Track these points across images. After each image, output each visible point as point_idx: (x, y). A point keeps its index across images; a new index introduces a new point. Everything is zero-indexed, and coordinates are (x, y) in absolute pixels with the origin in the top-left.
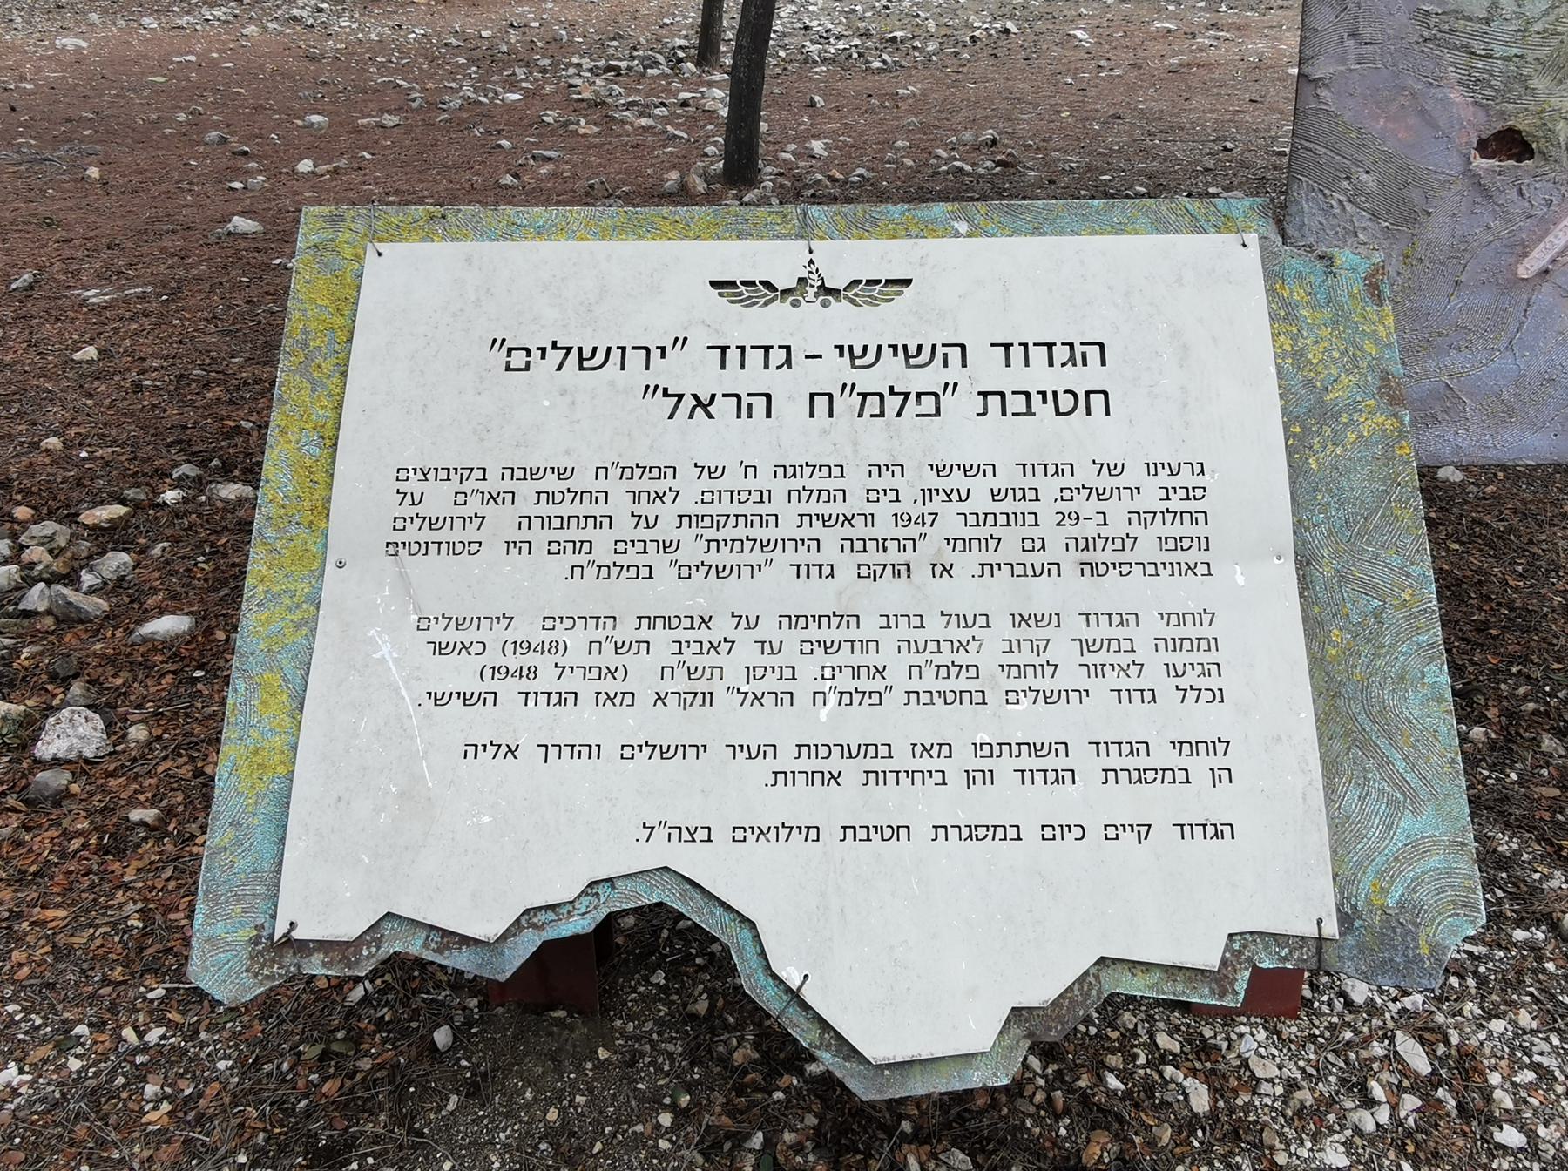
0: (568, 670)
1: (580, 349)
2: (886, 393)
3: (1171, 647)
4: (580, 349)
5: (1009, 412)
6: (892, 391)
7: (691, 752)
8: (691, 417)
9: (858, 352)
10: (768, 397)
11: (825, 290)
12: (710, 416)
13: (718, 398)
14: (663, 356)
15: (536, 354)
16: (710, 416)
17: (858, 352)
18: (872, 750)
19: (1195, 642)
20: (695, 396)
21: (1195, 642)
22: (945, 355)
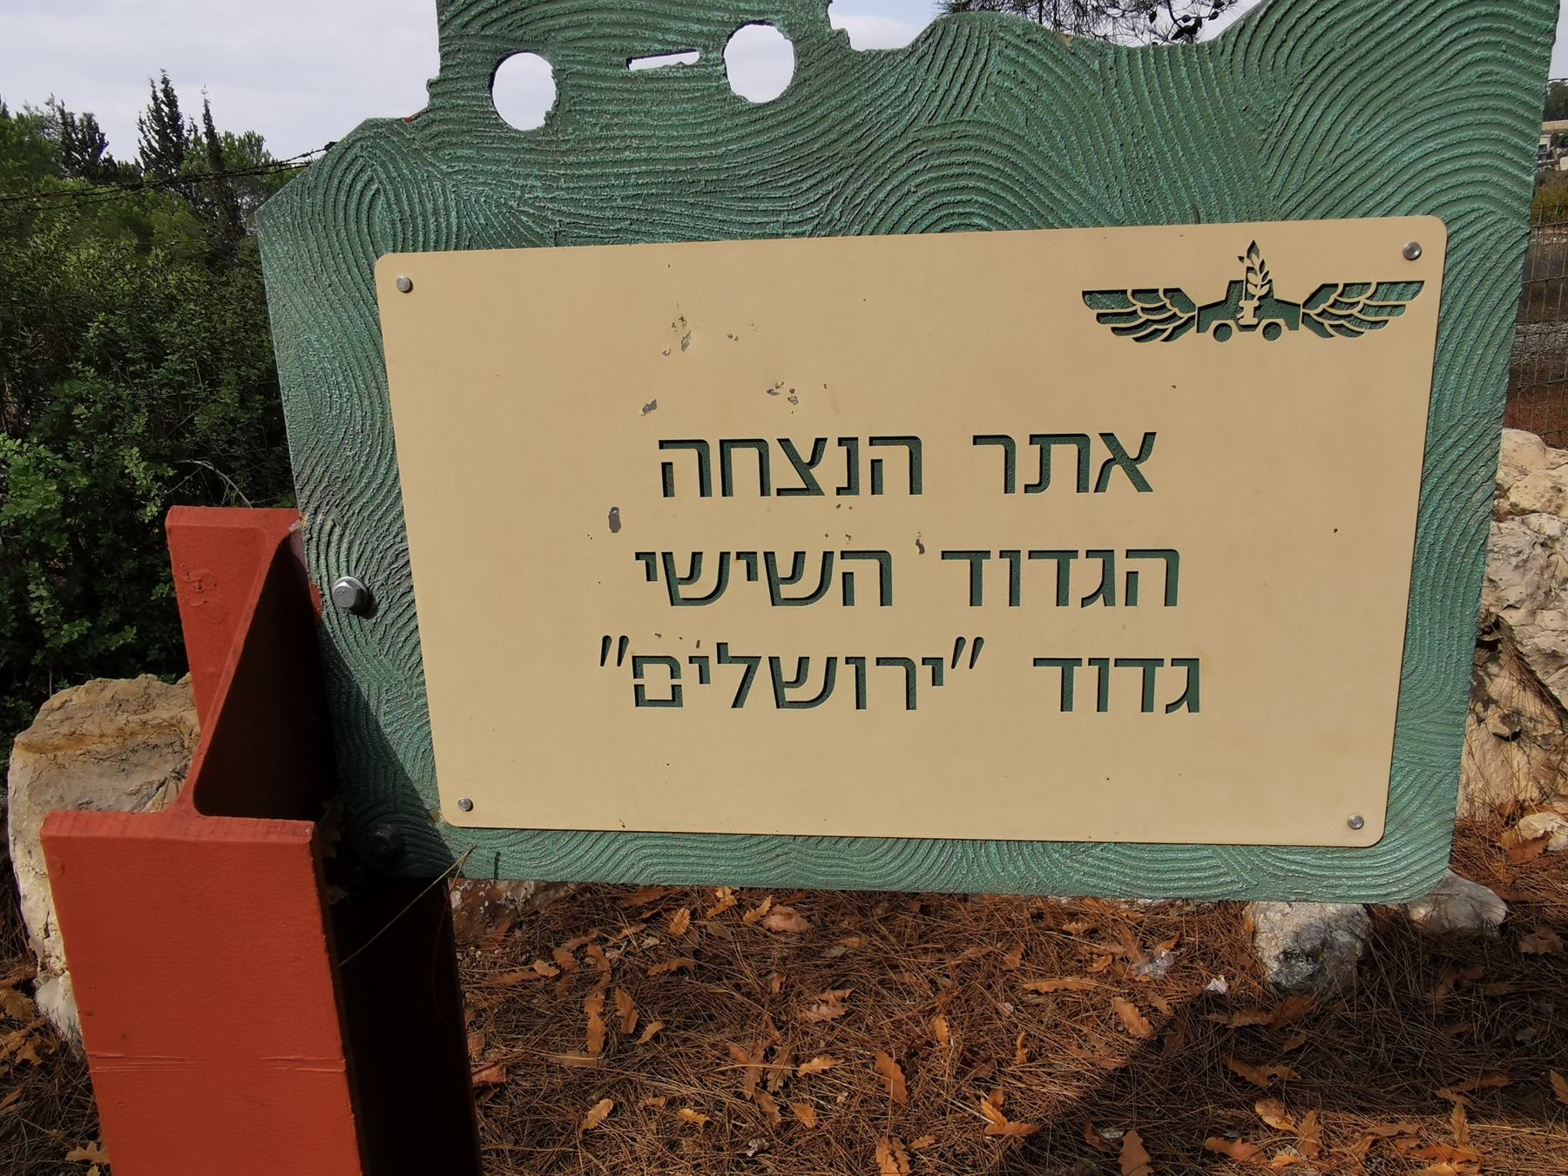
1: (774, 661)
4: (774, 661)
5: (669, 455)
9: (784, 568)
10: (1171, 556)
12: (1142, 485)
14: (936, 679)
15: (690, 672)
16: (1142, 485)
17: (784, 568)
20: (1108, 437)
22: (847, 577)
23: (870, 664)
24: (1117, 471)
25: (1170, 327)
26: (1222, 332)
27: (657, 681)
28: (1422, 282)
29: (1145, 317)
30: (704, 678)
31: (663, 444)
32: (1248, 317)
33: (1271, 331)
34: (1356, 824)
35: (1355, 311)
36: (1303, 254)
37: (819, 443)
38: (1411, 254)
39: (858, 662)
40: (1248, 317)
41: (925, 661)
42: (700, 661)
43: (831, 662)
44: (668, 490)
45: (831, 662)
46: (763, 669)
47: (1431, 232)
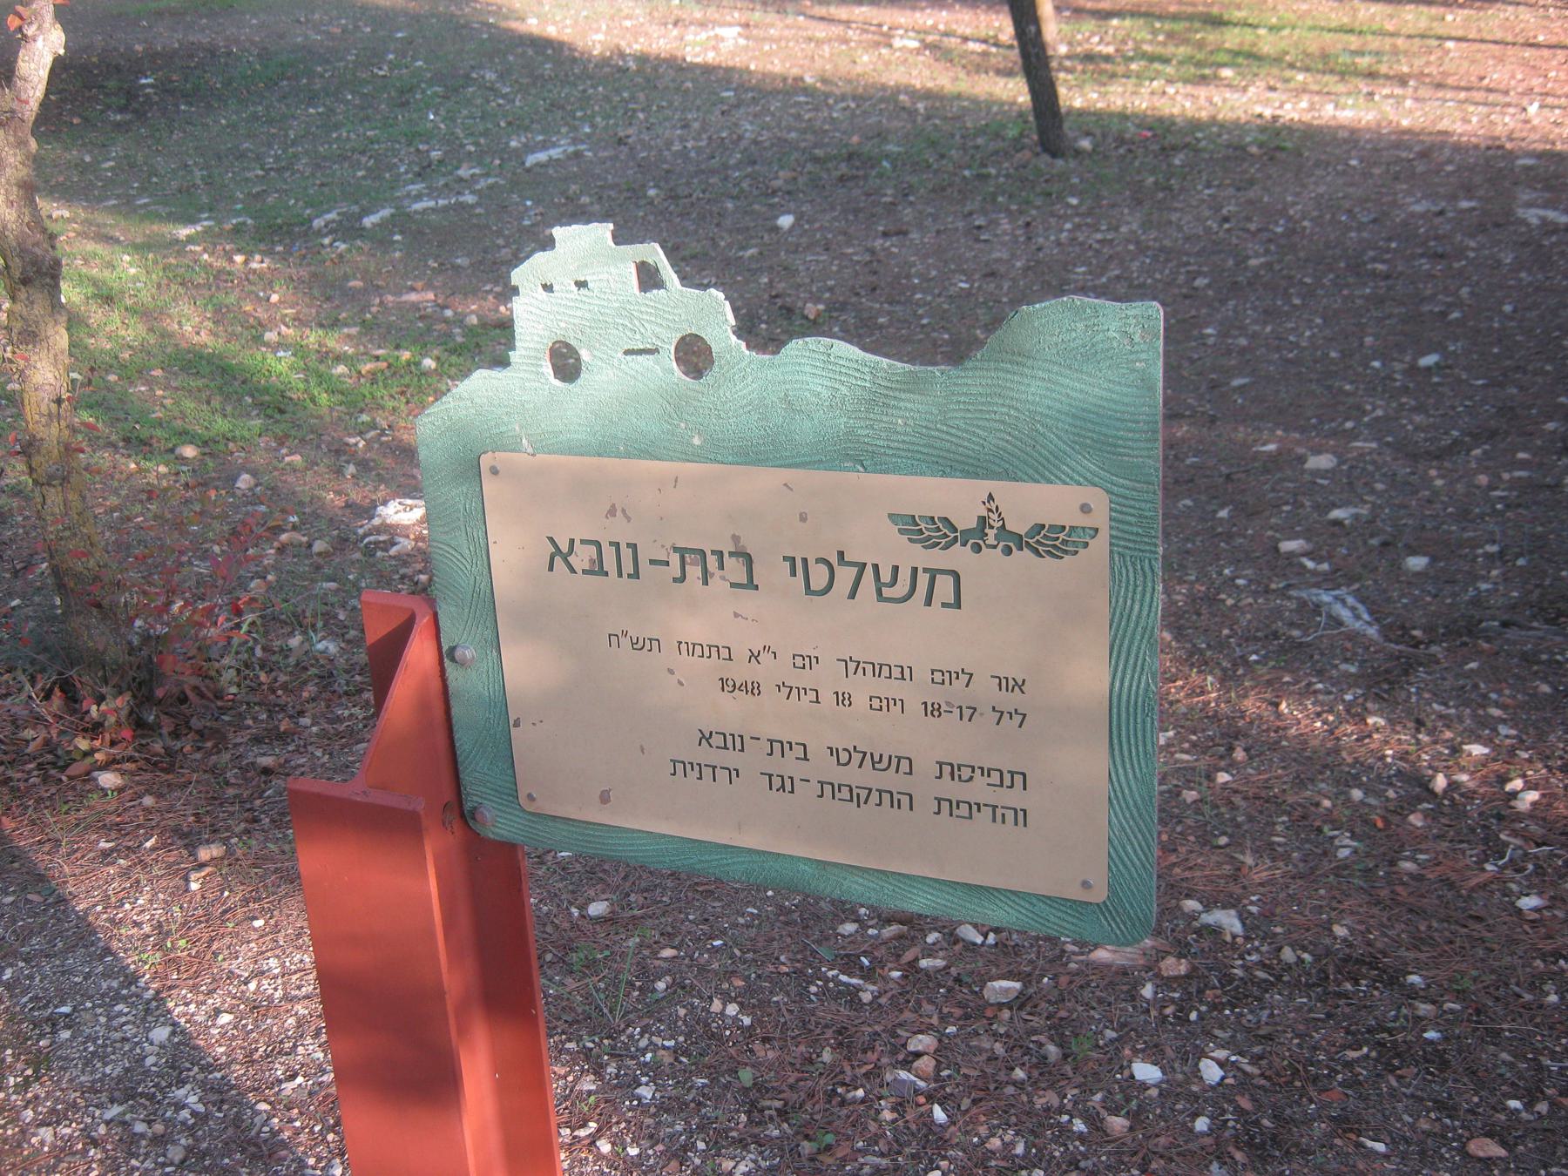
1: (876, 567)
2: (834, 560)
4: (876, 567)
8: (551, 568)
13: (577, 543)
23: (726, 555)
26: (977, 549)
28: (890, 516)
32: (991, 540)
33: (1008, 551)
37: (572, 541)
40: (991, 540)
41: (713, 552)
43: (915, 570)
45: (915, 570)
46: (869, 570)
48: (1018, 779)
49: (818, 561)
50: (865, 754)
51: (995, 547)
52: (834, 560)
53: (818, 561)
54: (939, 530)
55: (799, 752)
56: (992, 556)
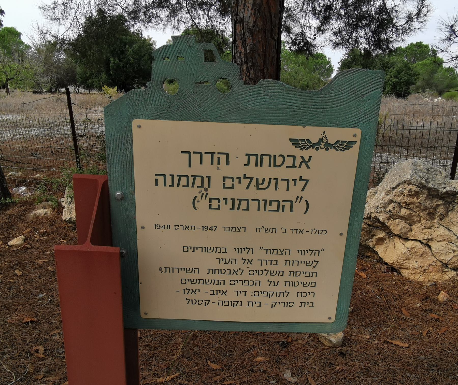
0: (278, 303)
1: (257, 179)
3: (169, 182)
4: (257, 179)
6: (286, 292)
7: (176, 270)
8: (310, 157)
11: (327, 144)
12: (308, 167)
15: (237, 181)
16: (308, 167)
18: (219, 250)
19: (191, 179)
21: (191, 179)
22: (219, 159)
23: (279, 181)
24: (303, 164)
25: (307, 147)
26: (317, 149)
27: (252, 273)
29: (302, 145)
30: (240, 182)
31: (156, 175)
34: (330, 318)
35: (343, 146)
36: (335, 134)
38: (355, 136)
39: (276, 180)
40: (322, 146)
42: (239, 178)
43: (270, 179)
44: (157, 184)
45: (270, 179)
46: (191, 301)
47: (358, 132)
48: (274, 230)
49: (280, 156)
50: (189, 300)
51: (323, 148)
52: (264, 270)
53: (280, 156)
54: (306, 143)
55: (258, 304)
56: (322, 152)
